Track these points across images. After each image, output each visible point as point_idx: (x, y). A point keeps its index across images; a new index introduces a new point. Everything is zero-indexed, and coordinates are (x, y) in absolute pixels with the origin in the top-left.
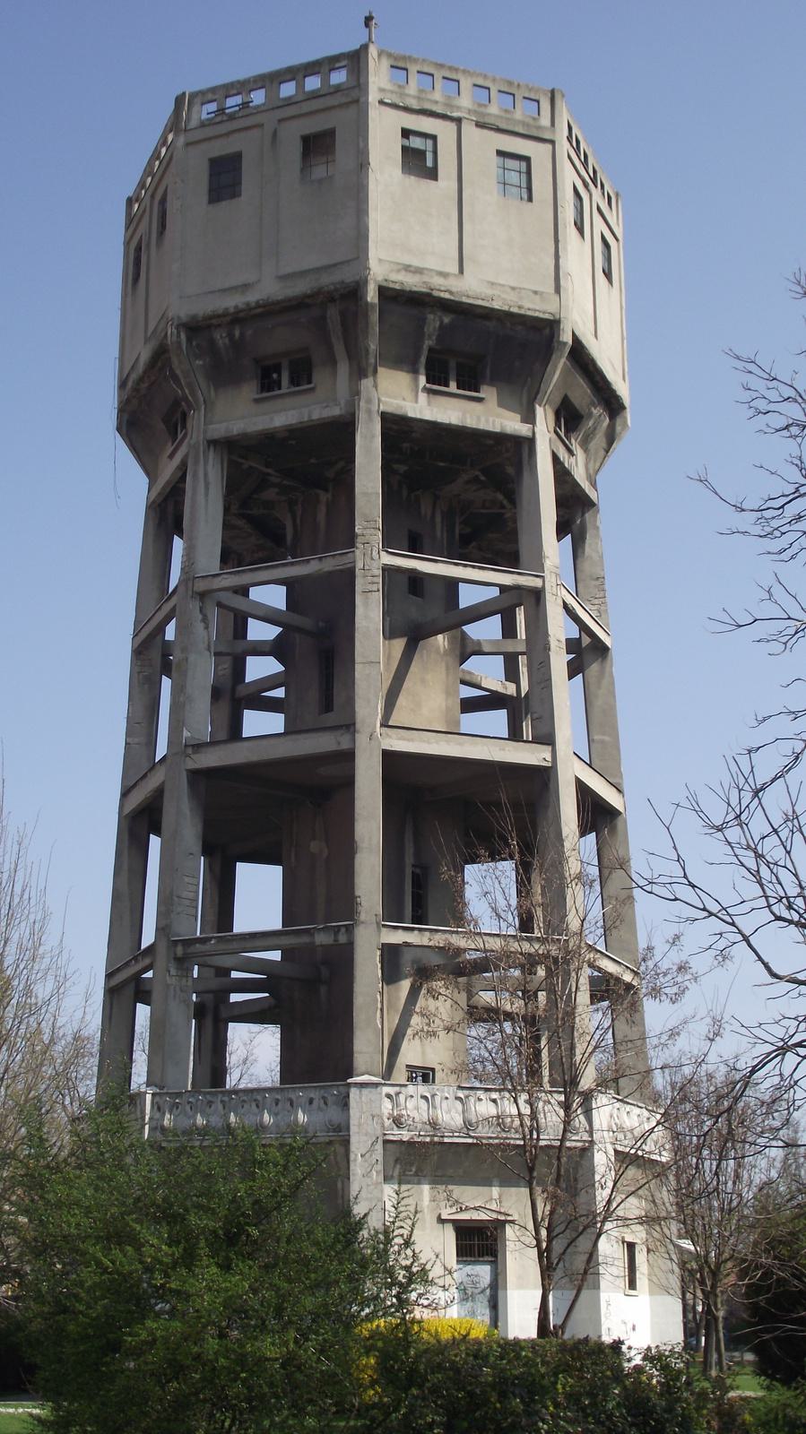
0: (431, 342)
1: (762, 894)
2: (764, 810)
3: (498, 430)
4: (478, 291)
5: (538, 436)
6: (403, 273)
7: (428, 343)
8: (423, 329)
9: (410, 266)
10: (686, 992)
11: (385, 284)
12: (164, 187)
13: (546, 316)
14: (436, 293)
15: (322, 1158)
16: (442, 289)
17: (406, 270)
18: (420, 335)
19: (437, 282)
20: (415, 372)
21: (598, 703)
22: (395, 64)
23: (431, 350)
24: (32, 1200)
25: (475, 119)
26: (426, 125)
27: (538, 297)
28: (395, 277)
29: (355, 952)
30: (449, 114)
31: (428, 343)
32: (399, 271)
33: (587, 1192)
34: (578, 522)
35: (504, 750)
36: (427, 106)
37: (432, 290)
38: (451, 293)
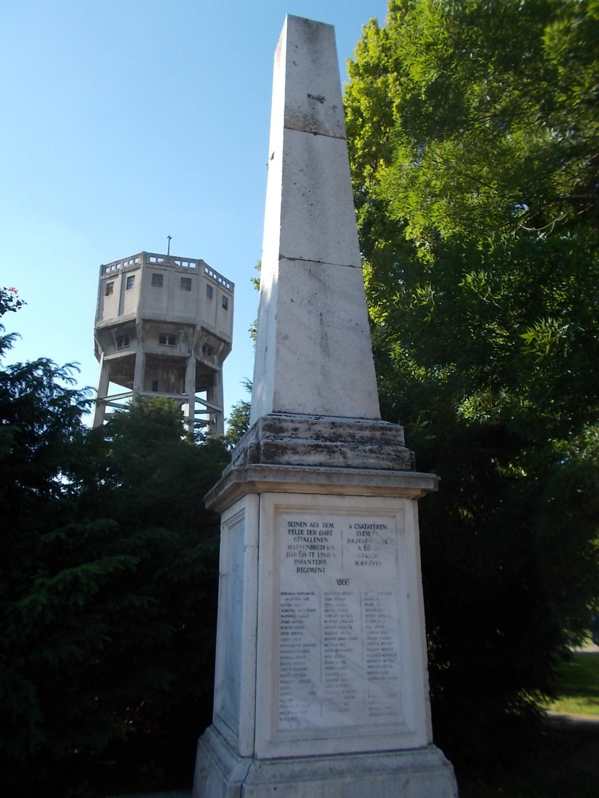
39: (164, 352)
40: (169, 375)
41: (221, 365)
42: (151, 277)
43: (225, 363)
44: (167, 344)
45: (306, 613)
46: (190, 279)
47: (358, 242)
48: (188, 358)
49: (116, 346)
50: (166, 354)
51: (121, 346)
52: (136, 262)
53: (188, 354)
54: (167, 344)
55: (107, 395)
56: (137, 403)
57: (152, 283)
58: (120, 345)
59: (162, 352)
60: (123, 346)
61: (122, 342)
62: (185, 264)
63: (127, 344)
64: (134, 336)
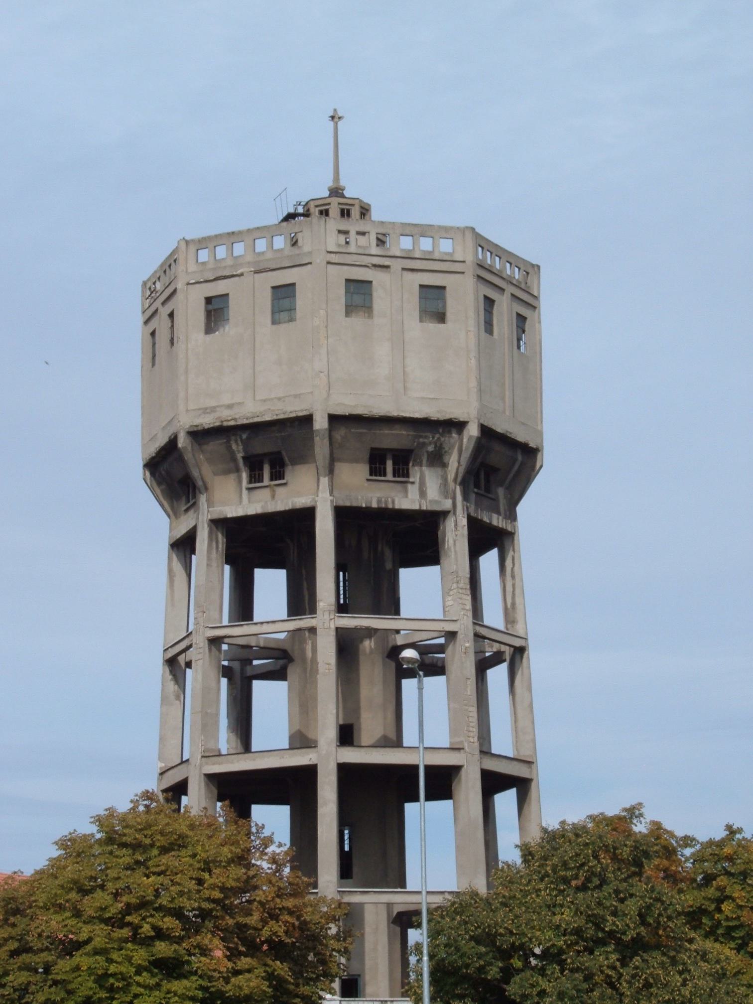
8: (232, 448)
9: (206, 409)
11: (191, 430)
12: (155, 309)
14: (225, 424)
15: (716, 857)
16: (229, 418)
17: (204, 413)
20: (238, 470)
23: (244, 458)
24: (79, 996)
25: (253, 269)
28: (197, 421)
29: (511, 775)
30: (235, 273)
34: (441, 528)
35: (283, 758)
36: (220, 274)
37: (222, 422)
38: (235, 419)
39: (386, 502)
40: (380, 548)
41: (512, 516)
42: (342, 291)
43: (520, 509)
44: (390, 476)
45: (165, 280)
46: (443, 288)
47: (365, 231)
48: (444, 514)
49: (245, 476)
50: (390, 506)
51: (262, 481)
52: (276, 247)
53: (447, 504)
54: (390, 476)
55: (221, 622)
56: (413, 944)
57: (347, 306)
58: (255, 477)
59: (379, 501)
60: (266, 481)
61: (261, 469)
62: (426, 244)
63: (278, 474)
64: (303, 456)
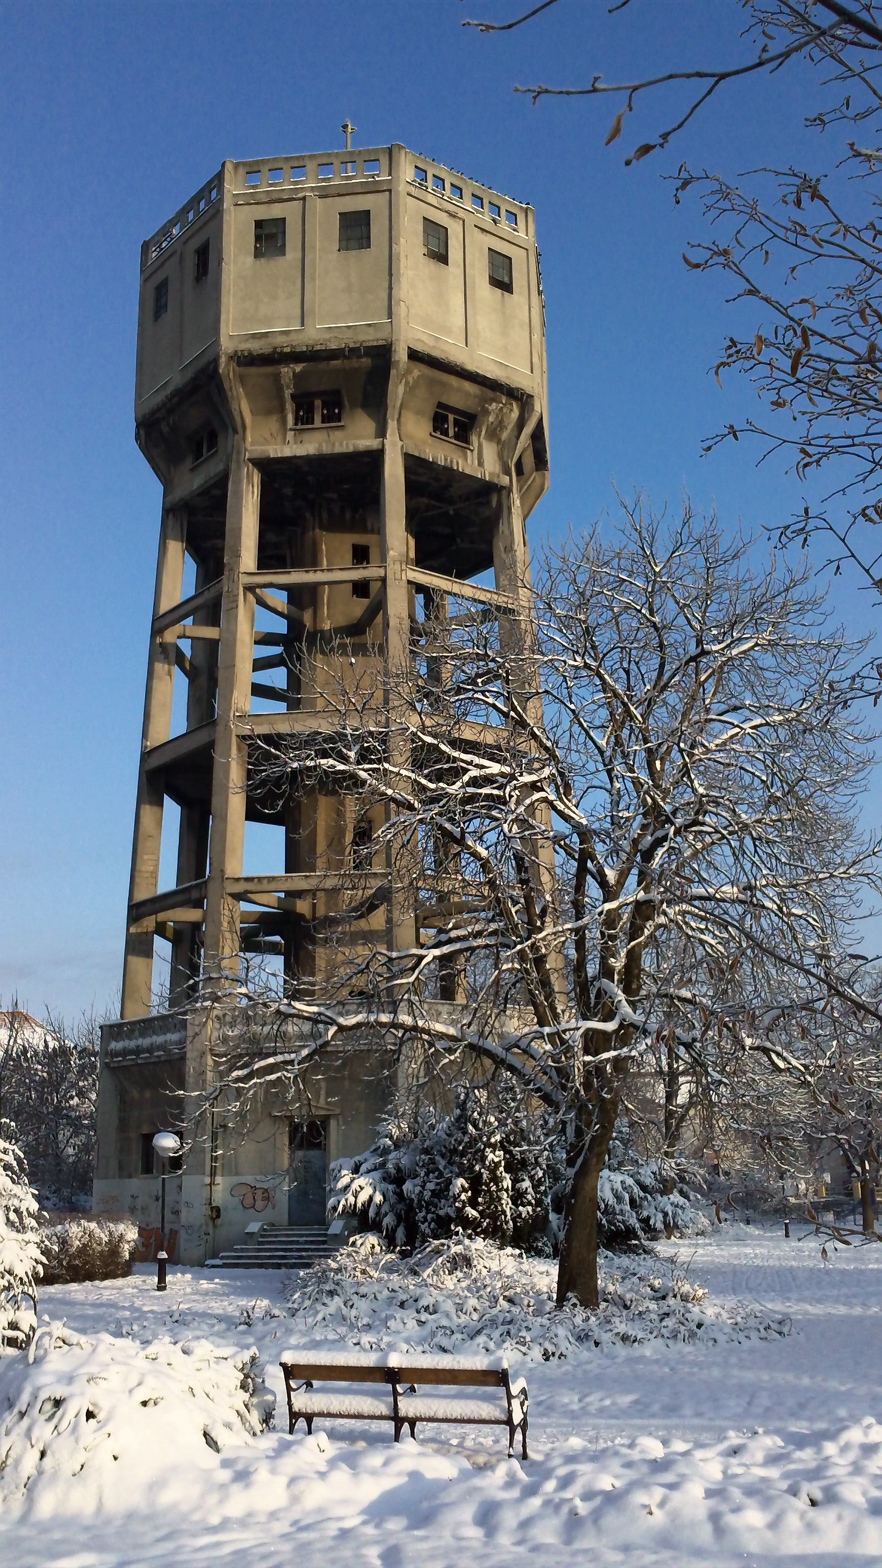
0: (290, 391)
1: (503, 1417)
2: (709, 92)
3: (351, 449)
4: (317, 338)
5: (387, 447)
6: (251, 340)
7: (288, 393)
10: (812, 117)
13: (381, 343)
18: (280, 389)
19: (280, 341)
21: (145, 858)
22: (249, 170)
23: (293, 397)
26: (276, 211)
27: (372, 328)
31: (288, 393)
32: (247, 340)
33: (147, 1225)
